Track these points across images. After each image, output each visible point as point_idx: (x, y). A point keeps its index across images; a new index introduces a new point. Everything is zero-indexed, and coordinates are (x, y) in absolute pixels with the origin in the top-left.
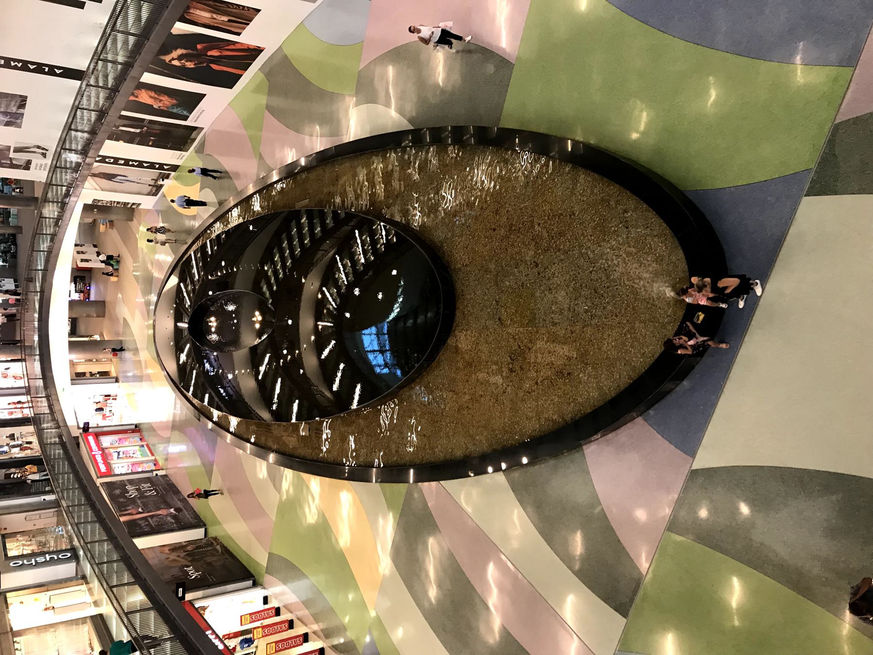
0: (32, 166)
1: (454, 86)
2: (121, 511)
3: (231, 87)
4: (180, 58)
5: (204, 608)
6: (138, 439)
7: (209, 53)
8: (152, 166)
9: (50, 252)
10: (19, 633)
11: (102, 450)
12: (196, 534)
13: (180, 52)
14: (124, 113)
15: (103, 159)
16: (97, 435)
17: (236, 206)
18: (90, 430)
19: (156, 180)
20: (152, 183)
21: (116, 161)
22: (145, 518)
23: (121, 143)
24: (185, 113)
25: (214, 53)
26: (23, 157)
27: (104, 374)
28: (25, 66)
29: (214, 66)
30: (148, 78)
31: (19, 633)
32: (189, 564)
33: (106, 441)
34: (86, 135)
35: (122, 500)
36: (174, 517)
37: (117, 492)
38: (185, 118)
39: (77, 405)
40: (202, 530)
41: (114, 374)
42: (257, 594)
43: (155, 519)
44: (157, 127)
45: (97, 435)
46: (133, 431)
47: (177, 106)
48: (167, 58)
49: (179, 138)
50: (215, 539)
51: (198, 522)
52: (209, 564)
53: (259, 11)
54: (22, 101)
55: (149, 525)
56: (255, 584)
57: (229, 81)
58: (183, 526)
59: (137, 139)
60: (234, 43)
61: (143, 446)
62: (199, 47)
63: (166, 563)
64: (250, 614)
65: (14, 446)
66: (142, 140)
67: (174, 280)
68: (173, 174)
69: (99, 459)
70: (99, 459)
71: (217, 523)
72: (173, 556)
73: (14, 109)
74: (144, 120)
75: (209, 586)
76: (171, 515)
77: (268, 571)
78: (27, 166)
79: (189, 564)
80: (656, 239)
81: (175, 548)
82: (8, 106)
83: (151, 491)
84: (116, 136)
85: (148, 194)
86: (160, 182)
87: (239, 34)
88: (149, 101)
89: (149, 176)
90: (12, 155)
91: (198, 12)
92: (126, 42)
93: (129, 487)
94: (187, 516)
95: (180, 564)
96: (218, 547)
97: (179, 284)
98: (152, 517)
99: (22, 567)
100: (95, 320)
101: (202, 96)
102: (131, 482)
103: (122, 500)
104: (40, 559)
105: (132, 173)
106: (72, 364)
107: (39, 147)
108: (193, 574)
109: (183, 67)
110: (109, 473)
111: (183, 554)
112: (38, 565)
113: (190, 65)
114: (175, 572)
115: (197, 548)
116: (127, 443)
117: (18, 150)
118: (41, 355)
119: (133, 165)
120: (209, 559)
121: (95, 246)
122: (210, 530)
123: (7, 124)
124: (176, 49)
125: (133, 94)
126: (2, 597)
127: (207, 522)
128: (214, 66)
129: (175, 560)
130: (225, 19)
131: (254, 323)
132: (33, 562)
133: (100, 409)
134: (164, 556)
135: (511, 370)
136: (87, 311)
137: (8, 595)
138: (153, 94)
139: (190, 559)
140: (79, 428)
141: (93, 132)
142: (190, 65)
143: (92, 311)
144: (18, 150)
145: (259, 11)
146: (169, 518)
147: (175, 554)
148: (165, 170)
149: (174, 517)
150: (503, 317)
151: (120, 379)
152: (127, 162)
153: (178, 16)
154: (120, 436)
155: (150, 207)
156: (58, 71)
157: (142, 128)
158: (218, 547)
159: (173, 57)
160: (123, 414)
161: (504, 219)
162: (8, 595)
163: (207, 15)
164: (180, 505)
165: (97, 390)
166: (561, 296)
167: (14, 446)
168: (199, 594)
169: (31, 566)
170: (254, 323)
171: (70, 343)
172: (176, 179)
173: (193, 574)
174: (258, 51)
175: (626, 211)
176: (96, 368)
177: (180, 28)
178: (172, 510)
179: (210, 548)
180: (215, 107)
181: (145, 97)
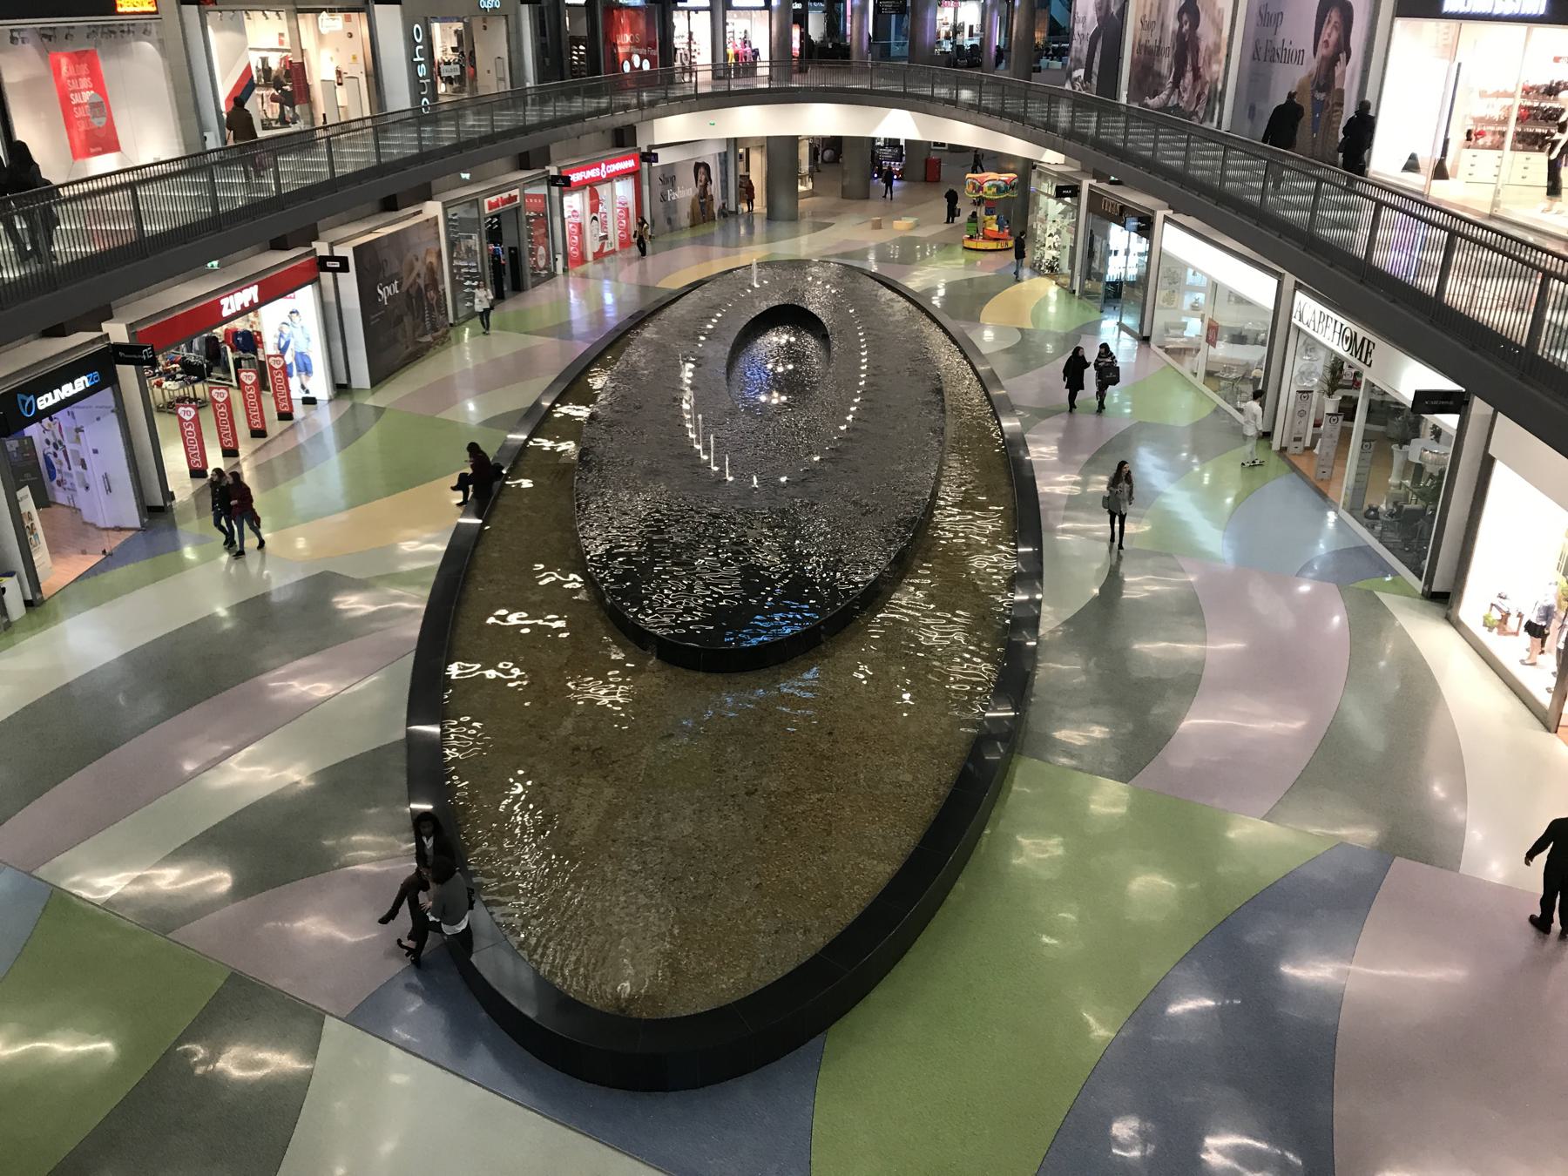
1: (590, 323)
16: (634, 174)
18: (645, 165)
32: (404, 289)
34: (1092, 131)
45: (634, 174)
52: (400, 320)
63: (410, 256)
72: (420, 267)
80: (743, 975)
92: (1253, 191)
95: (404, 275)
96: (428, 338)
99: (411, 42)
104: (422, 71)
108: (384, 293)
111: (421, 282)
112: (413, 66)
114: (394, 267)
118: (778, 90)
120: (408, 321)
126: (359, 4)
129: (412, 269)
131: (769, 393)
132: (419, 59)
134: (421, 254)
135: (577, 749)
139: (413, 292)
140: (651, 147)
141: (1097, 144)
147: (423, 271)
150: (673, 742)
154: (632, 211)
158: (428, 338)
161: (845, 749)
162: (363, 15)
166: (687, 828)
169: (411, 54)
170: (769, 393)
171: (794, 140)
173: (384, 293)
175: (807, 931)
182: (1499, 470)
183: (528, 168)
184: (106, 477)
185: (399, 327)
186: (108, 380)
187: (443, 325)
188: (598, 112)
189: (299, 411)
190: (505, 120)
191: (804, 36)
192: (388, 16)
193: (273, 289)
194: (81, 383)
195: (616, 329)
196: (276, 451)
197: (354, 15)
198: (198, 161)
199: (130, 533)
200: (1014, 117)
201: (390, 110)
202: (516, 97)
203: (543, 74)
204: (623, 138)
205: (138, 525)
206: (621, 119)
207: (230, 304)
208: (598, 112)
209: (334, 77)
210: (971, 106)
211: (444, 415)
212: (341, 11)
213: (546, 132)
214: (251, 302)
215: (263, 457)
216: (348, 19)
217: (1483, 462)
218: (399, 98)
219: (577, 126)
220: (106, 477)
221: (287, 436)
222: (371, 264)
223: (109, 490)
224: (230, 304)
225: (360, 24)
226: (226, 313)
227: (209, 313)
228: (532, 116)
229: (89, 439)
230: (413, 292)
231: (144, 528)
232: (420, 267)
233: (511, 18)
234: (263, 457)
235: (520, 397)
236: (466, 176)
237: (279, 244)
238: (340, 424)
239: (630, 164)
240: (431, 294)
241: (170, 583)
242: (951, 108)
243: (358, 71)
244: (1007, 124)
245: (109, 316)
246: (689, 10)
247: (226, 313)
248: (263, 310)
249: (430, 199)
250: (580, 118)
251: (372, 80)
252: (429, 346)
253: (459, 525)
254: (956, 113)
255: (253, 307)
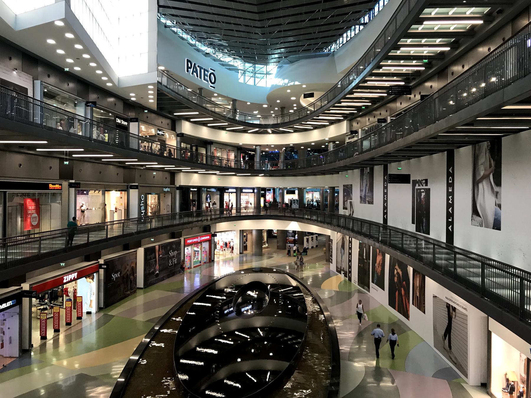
0: (345, 210)
2: (162, 247)
3: (389, 305)
4: (398, 273)
5: (93, 279)
6: (205, 260)
7: (402, 289)
8: (350, 267)
9: (285, 216)
10: (104, 194)
11: (201, 242)
12: (140, 282)
13: (400, 273)
14: (371, 247)
15: (350, 242)
16: (210, 241)
17: (320, 308)
19: (343, 270)
20: (342, 268)
21: (350, 248)
22: (155, 257)
23: (358, 250)
24: (375, 281)
25: (403, 292)
26: (348, 206)
27: (245, 248)
28: (385, 201)
29: (397, 293)
30: (388, 257)
31: (104, 194)
32: (122, 275)
33: (206, 245)
35: (169, 248)
36: (153, 273)
37: (174, 246)
38: (373, 282)
39: (227, 234)
40: (142, 287)
41: (245, 252)
42: (94, 310)
43: (154, 262)
44: (367, 267)
45: (210, 241)
46: (210, 259)
47: (378, 276)
48: (397, 267)
49: (363, 281)
50: (135, 292)
51: (148, 284)
52: (119, 286)
53: (424, 313)
54: (371, 202)
55: (151, 259)
56: (100, 309)
57: (392, 303)
58: (147, 276)
59: (360, 258)
60: (409, 302)
61: (200, 262)
62: (404, 283)
64: (82, 302)
65: (209, 204)
66: (361, 260)
67: (294, 283)
68: (347, 279)
69: (195, 240)
70: (195, 240)
71: (145, 293)
72: (128, 268)
73: (367, 199)
74: (370, 260)
75: (105, 283)
76: (155, 271)
77: (105, 315)
78: (345, 208)
79: (122, 275)
81: (134, 271)
82: (368, 196)
83: (172, 263)
84: (361, 246)
85: (337, 267)
86: (342, 272)
87: (413, 304)
88: (378, 261)
89: (345, 266)
90: (349, 201)
91: (418, 279)
93: (176, 252)
94: (152, 279)
96: (129, 292)
97: (292, 286)
98: (156, 261)
99: (140, 200)
100: (275, 245)
101: (383, 289)
102: (179, 254)
103: (169, 248)
104: (143, 208)
105: (346, 257)
106: (251, 231)
107: (353, 212)
109: (394, 276)
110: (186, 245)
112: (140, 207)
113: (396, 279)
115: (131, 282)
116: (203, 255)
117: (351, 203)
119: (349, 257)
120: (122, 287)
121: (317, 246)
122: (142, 291)
123: (361, 197)
124: (401, 271)
125: (380, 252)
127: (147, 289)
128: (397, 293)
130: (418, 295)
133: (226, 244)
136: (280, 240)
137: (126, 192)
138: (381, 262)
139: (125, 276)
142: (396, 279)
143: (280, 244)
144: (351, 203)
145: (424, 313)
146: (153, 270)
148: (348, 274)
149: (153, 273)
151: (241, 255)
152: (350, 254)
153: (417, 269)
154: (208, 252)
155: (331, 269)
156: (385, 216)
157: (366, 259)
158: (129, 292)
159: (398, 270)
160: (220, 255)
162: (126, 192)
163: (418, 285)
164: (160, 277)
165: (236, 243)
167: (209, 204)
168: (102, 277)
172: (345, 281)
174: (407, 316)
176: (249, 244)
177: (411, 270)
178: (157, 272)
179: (129, 288)
180: (379, 296)
181: (379, 258)
182: (494, 336)
183: (89, 261)
184: (10, 338)
185: (114, 292)
186: (19, 303)
187: (134, 288)
188: (198, 221)
189: (85, 316)
190: (166, 223)
191: (265, 201)
192: (134, 193)
193: (83, 274)
194: (9, 303)
195: (198, 289)
196: (73, 330)
197: (123, 192)
198: (120, 222)
199: (14, 359)
200: (328, 223)
201: (131, 218)
202: (173, 216)
203: (181, 209)
204: (206, 229)
205: (18, 356)
206: (205, 223)
207: (66, 279)
208: (198, 221)
209: (114, 210)
210: (315, 220)
211: (133, 318)
212: (119, 191)
213: (180, 227)
214: (74, 278)
215: (69, 332)
216: (121, 193)
217: (488, 333)
218: (134, 214)
219: (191, 225)
220: (10, 338)
221: (78, 325)
222: (110, 267)
223: (10, 343)
224: (66, 279)
225: (124, 194)
226: (65, 281)
227: (59, 282)
228: (177, 222)
229: (7, 324)
230: (125, 276)
231: (20, 356)
232: (128, 268)
233: (173, 194)
234: (69, 332)
235: (161, 312)
236: (63, 264)
237: (87, 259)
238: (98, 321)
239: (208, 237)
240: (132, 277)
241: (25, 377)
242: (310, 221)
243: (122, 208)
244: (326, 225)
245: (24, 281)
246: (229, 193)
247: (65, 281)
248: (78, 281)
249: (140, 247)
250: (191, 222)
251: (126, 211)
252: (129, 295)
253: (130, 360)
254: (311, 222)
255: (75, 280)
